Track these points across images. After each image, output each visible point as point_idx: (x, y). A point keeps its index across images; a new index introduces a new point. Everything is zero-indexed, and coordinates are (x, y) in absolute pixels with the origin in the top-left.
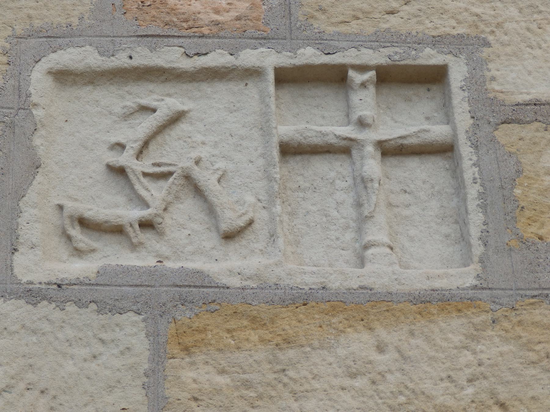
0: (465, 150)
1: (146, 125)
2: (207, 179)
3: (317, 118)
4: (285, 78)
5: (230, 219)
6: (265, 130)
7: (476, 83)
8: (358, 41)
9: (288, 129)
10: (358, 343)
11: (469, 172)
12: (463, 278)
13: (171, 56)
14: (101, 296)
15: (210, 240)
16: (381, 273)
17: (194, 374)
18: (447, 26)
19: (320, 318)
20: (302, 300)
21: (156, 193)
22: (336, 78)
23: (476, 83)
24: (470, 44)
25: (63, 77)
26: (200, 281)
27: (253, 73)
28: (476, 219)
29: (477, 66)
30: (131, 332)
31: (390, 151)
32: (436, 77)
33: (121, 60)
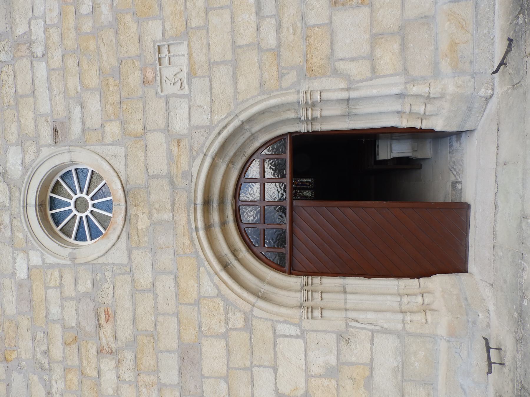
0: (169, 43)
1: (167, 81)
2: (174, 73)
3: (165, 61)
4: (160, 65)
5: (180, 70)
6: (167, 67)
7: (160, 41)
8: (155, 56)
9: (167, 64)
10: (194, 55)
11: (172, 42)
12: (186, 43)
13: (158, 79)
14: (190, 84)
15: (182, 73)
16: (186, 53)
17: (199, 73)
18: (152, 45)
19: (78, 92)
20: (189, 61)
21: (176, 79)
22: (160, 59)
23: (160, 41)
24: (154, 42)
25: (162, 91)
26: (188, 73)
27: (160, 69)
28: (178, 41)
29: (157, 41)
30: (194, 80)
31: (169, 53)
32: (159, 46)
33: (159, 84)
